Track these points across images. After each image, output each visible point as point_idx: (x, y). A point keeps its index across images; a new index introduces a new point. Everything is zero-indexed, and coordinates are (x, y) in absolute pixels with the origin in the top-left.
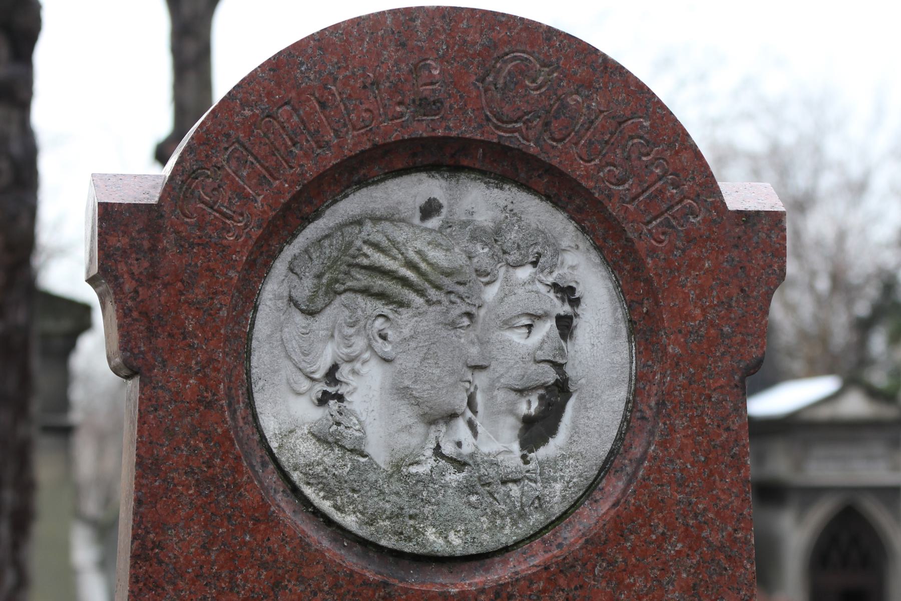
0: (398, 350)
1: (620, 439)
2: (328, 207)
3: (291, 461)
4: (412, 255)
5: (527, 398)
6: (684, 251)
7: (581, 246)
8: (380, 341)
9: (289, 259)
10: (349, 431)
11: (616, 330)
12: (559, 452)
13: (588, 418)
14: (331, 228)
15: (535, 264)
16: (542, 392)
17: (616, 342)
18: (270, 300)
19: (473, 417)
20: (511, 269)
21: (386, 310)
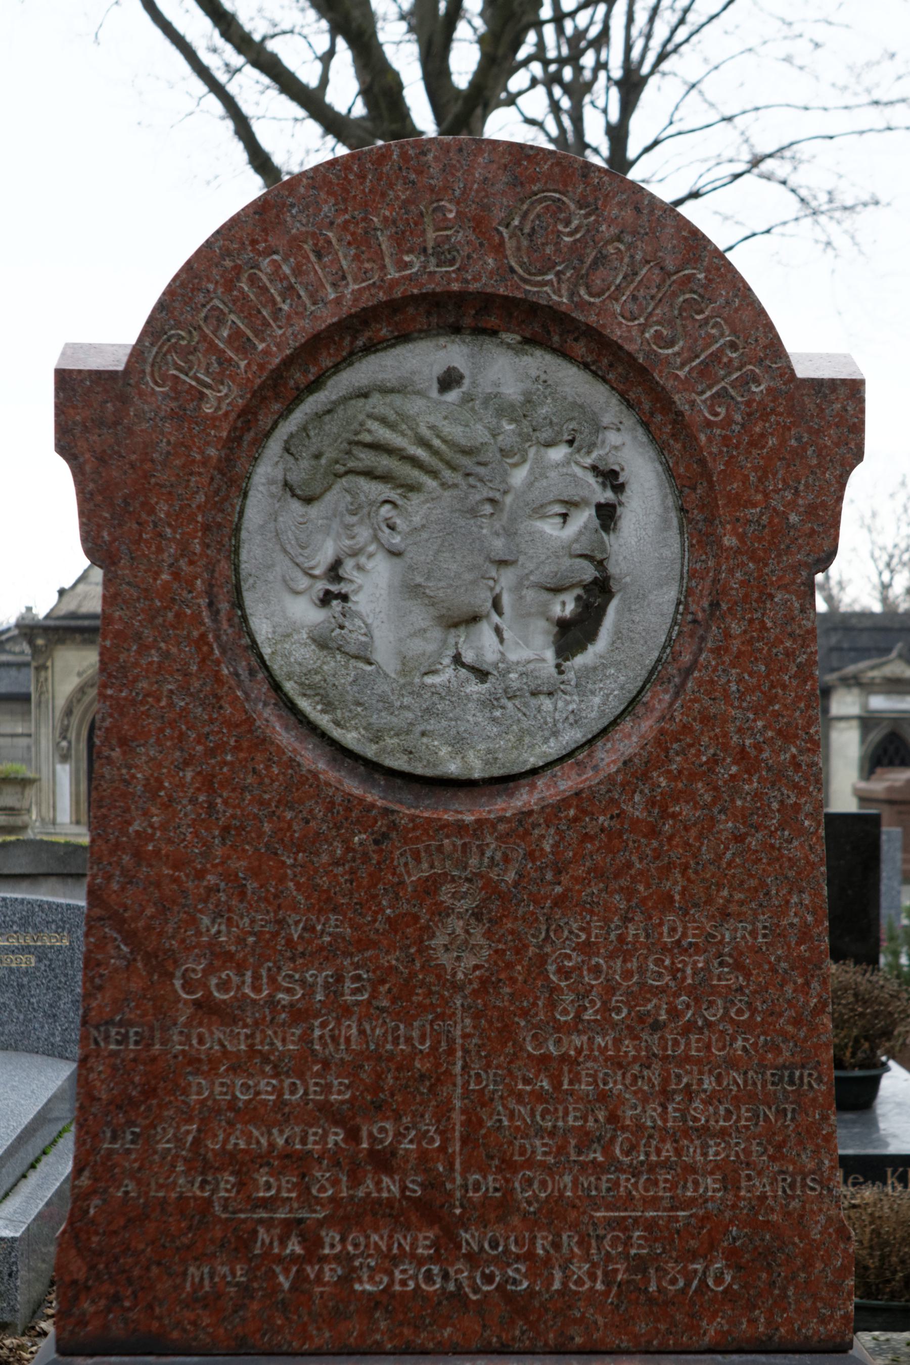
0: (409, 541)
6: (743, 426)
8: (387, 530)
9: (285, 438)
10: (354, 636)
11: (666, 520)
12: (598, 661)
14: (334, 402)
15: (571, 443)
17: (665, 534)
18: (263, 484)
20: (542, 449)
21: (394, 495)
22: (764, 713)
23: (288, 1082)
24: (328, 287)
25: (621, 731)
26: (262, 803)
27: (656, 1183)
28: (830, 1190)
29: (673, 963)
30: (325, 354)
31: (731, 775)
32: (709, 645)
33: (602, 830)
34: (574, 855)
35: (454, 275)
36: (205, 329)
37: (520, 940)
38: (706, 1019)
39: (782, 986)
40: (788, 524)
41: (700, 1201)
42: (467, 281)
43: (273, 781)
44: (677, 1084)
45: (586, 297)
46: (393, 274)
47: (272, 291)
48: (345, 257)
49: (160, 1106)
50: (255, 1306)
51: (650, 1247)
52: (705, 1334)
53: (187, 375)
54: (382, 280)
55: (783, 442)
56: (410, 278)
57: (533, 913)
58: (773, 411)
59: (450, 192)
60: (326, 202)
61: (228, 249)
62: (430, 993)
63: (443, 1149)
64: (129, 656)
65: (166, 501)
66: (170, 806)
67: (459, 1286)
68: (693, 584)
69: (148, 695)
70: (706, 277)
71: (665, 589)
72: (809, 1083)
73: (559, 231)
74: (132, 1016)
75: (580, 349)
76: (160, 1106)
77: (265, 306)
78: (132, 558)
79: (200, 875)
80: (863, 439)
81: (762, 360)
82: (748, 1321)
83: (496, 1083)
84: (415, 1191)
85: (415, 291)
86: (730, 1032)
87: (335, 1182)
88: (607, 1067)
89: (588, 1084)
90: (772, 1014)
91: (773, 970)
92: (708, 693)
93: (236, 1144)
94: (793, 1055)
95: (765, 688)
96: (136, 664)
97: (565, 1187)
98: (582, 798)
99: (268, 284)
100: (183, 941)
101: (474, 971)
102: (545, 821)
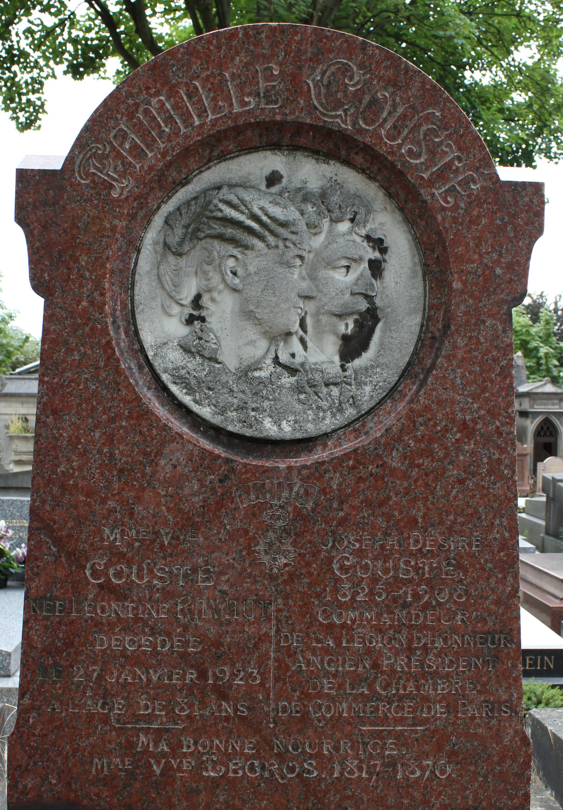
1: (416, 354)
2: (195, 176)
3: (162, 365)
4: (256, 210)
5: (346, 321)
7: (388, 208)
9: (166, 215)
11: (414, 272)
12: (369, 363)
13: (392, 337)
16: (356, 317)
19: (304, 335)
20: (334, 224)
21: (235, 252)
22: (479, 399)
23: (160, 639)
24: (195, 117)
25: (385, 409)
26: (146, 454)
27: (403, 708)
28: (517, 713)
29: (417, 564)
30: (192, 160)
31: (456, 440)
32: (443, 353)
33: (371, 475)
34: (352, 491)
35: (277, 110)
36: (114, 143)
37: (315, 547)
38: (438, 601)
39: (488, 579)
40: (495, 274)
41: (432, 720)
42: (286, 115)
43: (153, 439)
44: (418, 644)
45: (364, 126)
46: (237, 109)
47: (159, 119)
48: (206, 99)
49: (76, 653)
50: (138, 785)
51: (398, 750)
52: (433, 806)
53: (102, 173)
54: (231, 113)
55: (492, 221)
56: (248, 112)
57: (324, 530)
58: (485, 202)
59: (276, 58)
60: (195, 63)
61: (131, 93)
62: (256, 582)
63: (262, 684)
64: (60, 356)
65: (86, 254)
66: (85, 455)
67: (272, 774)
68: (432, 313)
69: (72, 381)
70: (441, 115)
71: (413, 316)
72: (505, 643)
73: (346, 84)
74: (58, 594)
75: (359, 159)
76: (76, 653)
77: (153, 129)
78: (63, 291)
79: (104, 501)
80: (543, 221)
81: (478, 168)
82: (462, 798)
83: (298, 641)
84: (244, 712)
85: (252, 120)
86: (454, 609)
87: (191, 706)
88: (372, 632)
89: (360, 643)
90: (481, 598)
91: (483, 569)
92: (441, 385)
93: (126, 679)
94: (494, 625)
95: (480, 382)
96: (64, 361)
97: (343, 710)
98: (358, 454)
99: (156, 116)
100: (92, 544)
101: (285, 567)
102: (333, 469)
